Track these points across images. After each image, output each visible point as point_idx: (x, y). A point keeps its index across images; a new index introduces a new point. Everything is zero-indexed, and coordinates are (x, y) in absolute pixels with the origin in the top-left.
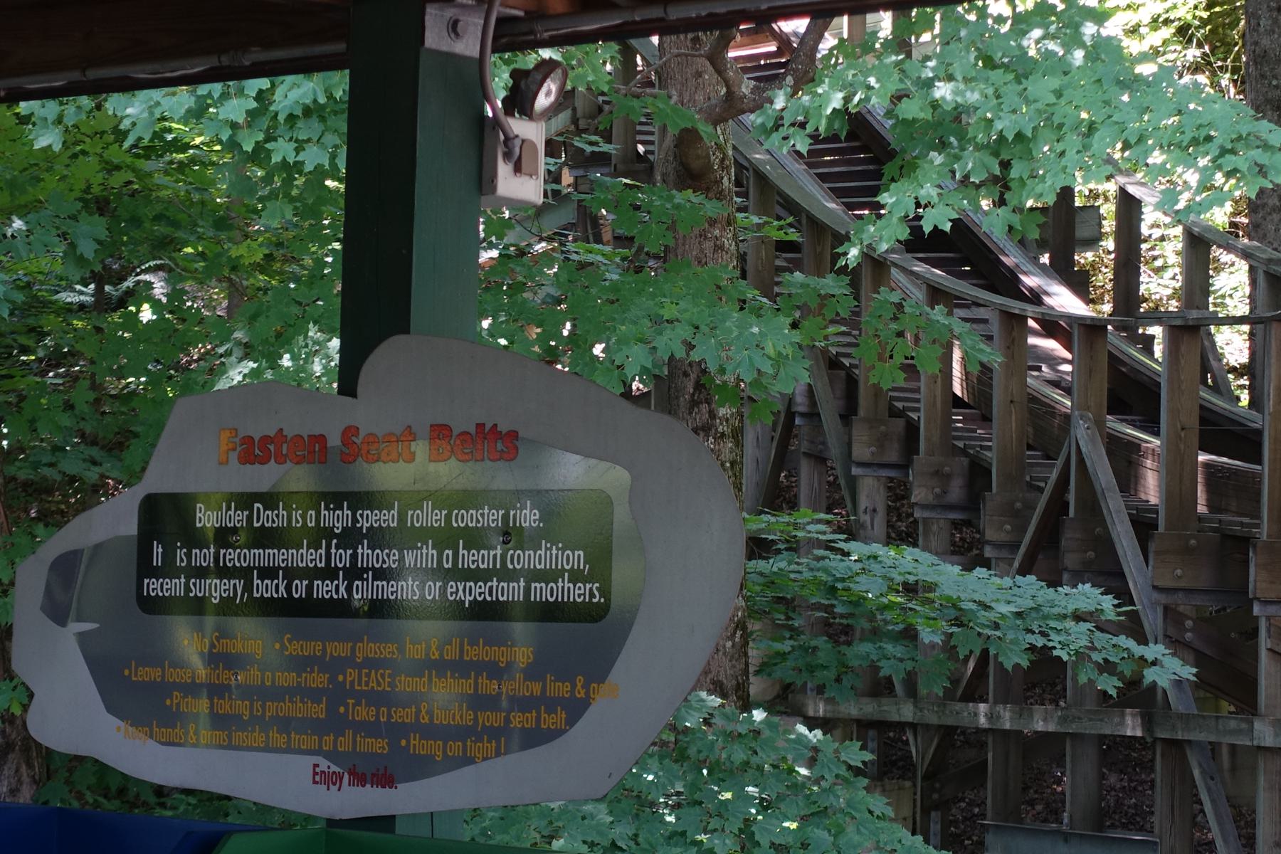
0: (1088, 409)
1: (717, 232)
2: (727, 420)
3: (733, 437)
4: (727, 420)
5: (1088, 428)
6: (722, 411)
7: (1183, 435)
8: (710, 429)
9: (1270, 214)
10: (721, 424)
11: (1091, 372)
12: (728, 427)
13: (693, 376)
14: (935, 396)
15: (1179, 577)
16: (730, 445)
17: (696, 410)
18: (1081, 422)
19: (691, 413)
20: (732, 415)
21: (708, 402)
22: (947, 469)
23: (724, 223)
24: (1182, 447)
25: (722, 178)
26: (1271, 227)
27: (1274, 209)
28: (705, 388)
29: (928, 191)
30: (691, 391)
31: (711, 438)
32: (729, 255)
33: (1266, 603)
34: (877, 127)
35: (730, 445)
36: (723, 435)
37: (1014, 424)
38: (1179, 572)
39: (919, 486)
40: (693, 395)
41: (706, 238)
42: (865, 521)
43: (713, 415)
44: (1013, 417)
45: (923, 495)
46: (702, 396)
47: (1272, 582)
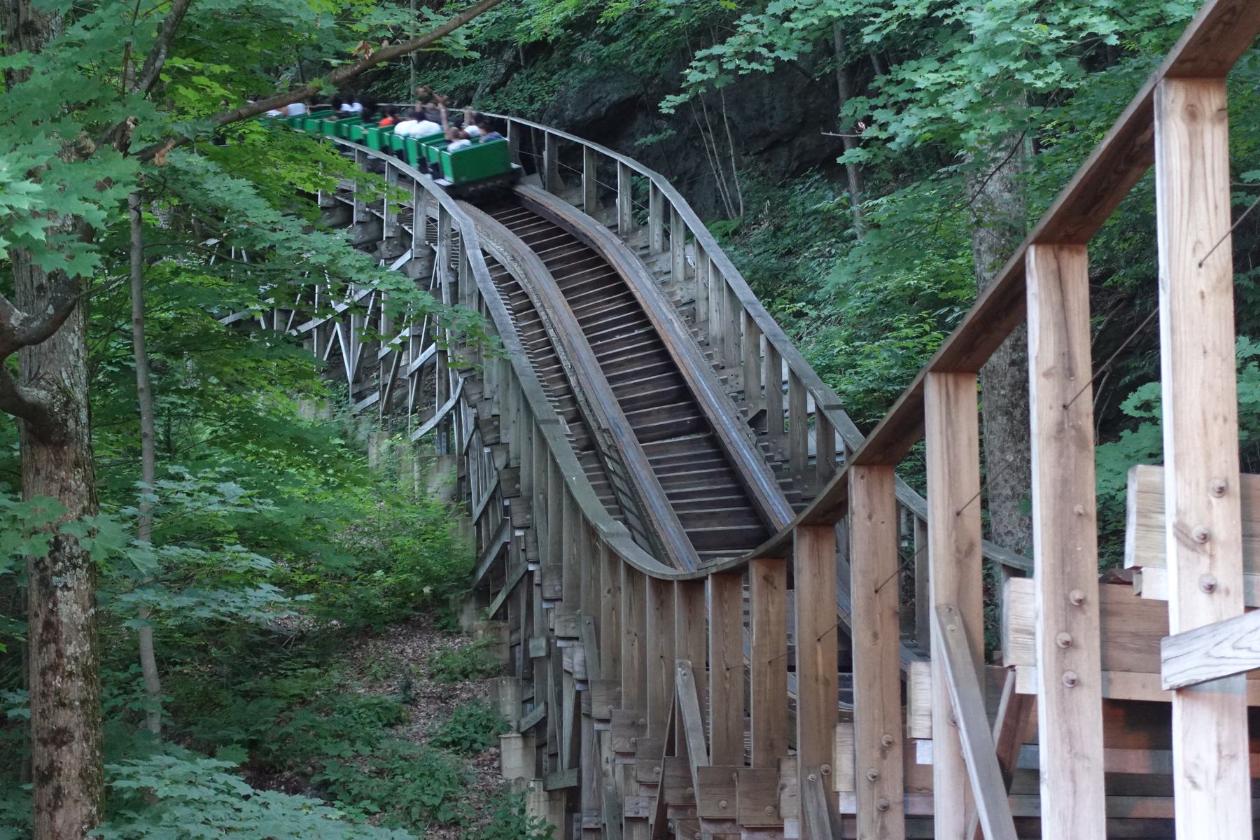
0: (689, 657)
1: (63, 474)
2: (76, 659)
4: (76, 659)
5: (685, 675)
6: (70, 650)
7: (728, 675)
10: (69, 663)
11: (690, 624)
12: (77, 666)
13: (42, 617)
14: (633, 657)
16: (80, 683)
17: (45, 650)
18: (680, 669)
19: (40, 653)
20: (83, 653)
21: (56, 641)
22: (642, 720)
23: (70, 465)
24: (727, 686)
25: (66, 420)
26: (1005, 513)
27: (1007, 498)
29: (405, 444)
30: (40, 631)
31: (58, 677)
32: (77, 496)
35: (80, 683)
36: (71, 674)
38: (723, 803)
39: (617, 736)
40: (42, 635)
41: (53, 480)
42: (607, 770)
43: (60, 654)
45: (621, 744)
46: (49, 636)
47: (755, 810)
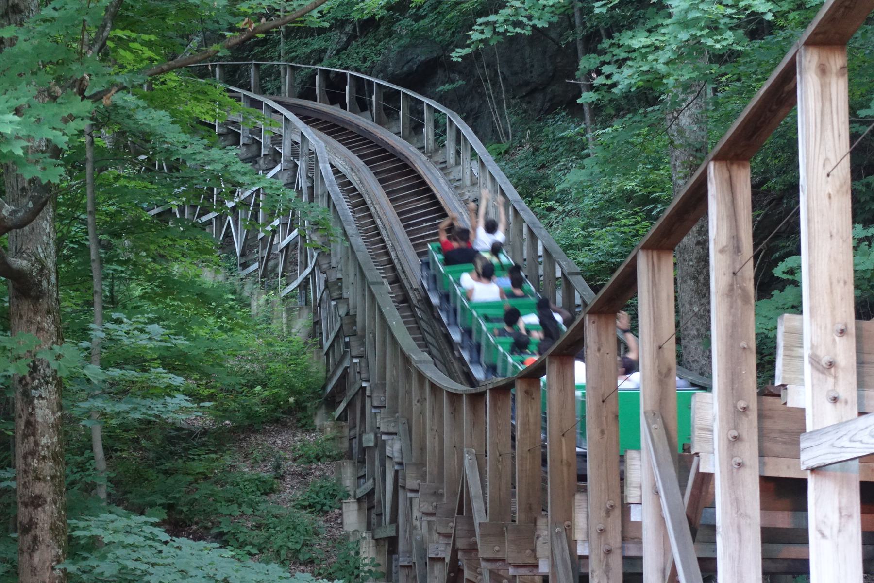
0: (473, 447)
1: (39, 318)
2: (48, 447)
3: (54, 458)
4: (48, 447)
6: (44, 441)
8: (35, 454)
9: (692, 340)
10: (43, 450)
12: (49, 452)
13: (24, 418)
15: (498, 551)
17: (26, 440)
19: (23, 443)
21: (34, 435)
22: (441, 490)
24: (500, 467)
25: (41, 282)
28: (32, 426)
31: (35, 460)
33: (517, 566)
34: (595, 301)
36: (44, 457)
37: (456, 460)
38: (497, 548)
41: (31, 323)
43: (36, 444)
44: (456, 456)
45: (426, 507)
